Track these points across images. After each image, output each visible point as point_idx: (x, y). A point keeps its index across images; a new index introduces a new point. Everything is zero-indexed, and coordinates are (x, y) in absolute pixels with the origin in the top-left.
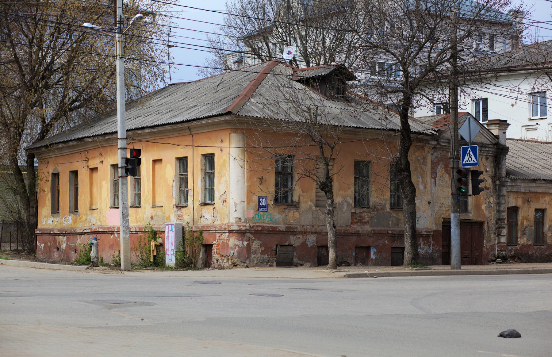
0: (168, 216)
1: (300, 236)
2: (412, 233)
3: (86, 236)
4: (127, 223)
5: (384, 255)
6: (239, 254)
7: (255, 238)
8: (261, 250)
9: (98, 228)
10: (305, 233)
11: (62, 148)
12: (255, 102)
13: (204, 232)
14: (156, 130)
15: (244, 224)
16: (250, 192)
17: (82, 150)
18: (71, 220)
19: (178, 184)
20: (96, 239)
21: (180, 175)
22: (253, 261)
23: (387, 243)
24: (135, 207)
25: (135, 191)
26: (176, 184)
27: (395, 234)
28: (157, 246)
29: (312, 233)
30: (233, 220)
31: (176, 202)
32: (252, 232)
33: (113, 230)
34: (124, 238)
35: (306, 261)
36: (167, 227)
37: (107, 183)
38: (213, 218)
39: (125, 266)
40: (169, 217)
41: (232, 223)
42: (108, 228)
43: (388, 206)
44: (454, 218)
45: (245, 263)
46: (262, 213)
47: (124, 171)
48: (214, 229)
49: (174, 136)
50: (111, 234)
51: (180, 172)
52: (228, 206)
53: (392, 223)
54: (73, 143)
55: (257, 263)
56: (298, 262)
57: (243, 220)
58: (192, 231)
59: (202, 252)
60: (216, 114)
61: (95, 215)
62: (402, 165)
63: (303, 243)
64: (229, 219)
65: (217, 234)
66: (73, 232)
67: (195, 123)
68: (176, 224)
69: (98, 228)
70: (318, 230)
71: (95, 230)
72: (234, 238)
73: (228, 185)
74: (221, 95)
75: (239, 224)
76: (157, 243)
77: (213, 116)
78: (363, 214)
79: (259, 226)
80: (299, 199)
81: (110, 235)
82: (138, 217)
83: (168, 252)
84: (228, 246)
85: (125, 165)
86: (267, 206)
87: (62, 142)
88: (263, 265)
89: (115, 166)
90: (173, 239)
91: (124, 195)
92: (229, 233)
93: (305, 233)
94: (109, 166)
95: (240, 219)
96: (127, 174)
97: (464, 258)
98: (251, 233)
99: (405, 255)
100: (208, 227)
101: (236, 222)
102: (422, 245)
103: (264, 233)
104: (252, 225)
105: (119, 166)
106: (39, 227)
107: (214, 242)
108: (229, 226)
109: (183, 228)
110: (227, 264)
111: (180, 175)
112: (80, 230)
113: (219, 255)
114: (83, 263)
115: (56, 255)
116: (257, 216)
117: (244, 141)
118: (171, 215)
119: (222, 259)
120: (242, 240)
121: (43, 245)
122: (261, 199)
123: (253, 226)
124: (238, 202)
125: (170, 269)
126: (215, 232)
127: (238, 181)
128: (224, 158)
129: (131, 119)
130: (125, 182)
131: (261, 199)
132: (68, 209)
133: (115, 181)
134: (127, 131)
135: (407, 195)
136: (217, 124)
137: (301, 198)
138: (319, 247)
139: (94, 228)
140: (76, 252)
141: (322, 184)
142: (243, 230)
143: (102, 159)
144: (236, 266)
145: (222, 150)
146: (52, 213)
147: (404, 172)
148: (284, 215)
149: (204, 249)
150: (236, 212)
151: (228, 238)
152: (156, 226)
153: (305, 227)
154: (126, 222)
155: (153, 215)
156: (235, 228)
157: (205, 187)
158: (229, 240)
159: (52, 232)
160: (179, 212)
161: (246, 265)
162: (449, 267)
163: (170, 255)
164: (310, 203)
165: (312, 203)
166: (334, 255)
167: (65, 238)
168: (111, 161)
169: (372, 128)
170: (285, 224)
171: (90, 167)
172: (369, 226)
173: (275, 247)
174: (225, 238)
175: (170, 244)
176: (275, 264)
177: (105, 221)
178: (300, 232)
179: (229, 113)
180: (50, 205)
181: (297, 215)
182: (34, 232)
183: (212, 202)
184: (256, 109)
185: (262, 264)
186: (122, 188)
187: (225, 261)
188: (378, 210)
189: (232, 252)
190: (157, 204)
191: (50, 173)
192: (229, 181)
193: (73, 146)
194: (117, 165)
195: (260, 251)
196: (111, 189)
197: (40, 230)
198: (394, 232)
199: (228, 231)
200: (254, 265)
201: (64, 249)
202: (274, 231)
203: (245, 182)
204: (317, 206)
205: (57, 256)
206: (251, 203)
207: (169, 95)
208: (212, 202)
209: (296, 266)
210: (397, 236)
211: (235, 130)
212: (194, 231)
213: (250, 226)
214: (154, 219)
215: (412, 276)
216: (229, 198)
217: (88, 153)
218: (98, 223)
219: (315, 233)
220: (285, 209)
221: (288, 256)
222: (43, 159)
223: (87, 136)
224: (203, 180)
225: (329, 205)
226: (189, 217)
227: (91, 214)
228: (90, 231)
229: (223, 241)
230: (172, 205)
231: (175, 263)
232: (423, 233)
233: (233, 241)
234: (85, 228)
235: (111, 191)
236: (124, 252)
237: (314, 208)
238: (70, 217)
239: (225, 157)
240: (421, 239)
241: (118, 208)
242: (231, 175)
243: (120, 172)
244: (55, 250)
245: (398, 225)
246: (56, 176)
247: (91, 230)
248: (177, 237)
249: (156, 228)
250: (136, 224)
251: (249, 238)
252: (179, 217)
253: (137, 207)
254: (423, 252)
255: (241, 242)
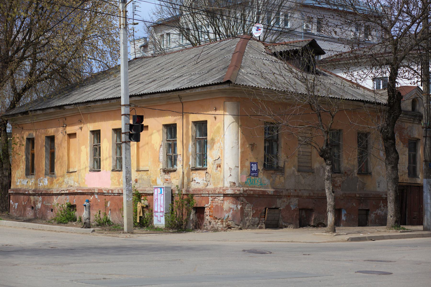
0: (154, 179)
1: (285, 200)
2: (395, 198)
3: (63, 197)
4: (130, 187)
5: (353, 217)
6: (234, 216)
7: (247, 201)
8: (253, 213)
9: (77, 190)
10: (289, 196)
11: (38, 115)
12: (246, 72)
13: (195, 195)
14: (144, 98)
15: (239, 189)
16: (243, 157)
17: (59, 117)
18: (47, 182)
19: (165, 149)
20: (88, 201)
21: (167, 141)
22: (246, 223)
23: (355, 205)
24: (117, 171)
25: (117, 156)
26: (163, 149)
27: (361, 198)
28: (143, 207)
29: (295, 196)
30: (227, 185)
31: (163, 167)
32: (245, 196)
33: (93, 192)
34: (127, 201)
35: (290, 224)
36: (156, 190)
37: (86, 147)
38: (205, 182)
39: (128, 229)
40: (156, 180)
41: (227, 187)
42: (87, 190)
43: (356, 171)
44: (427, 183)
45: (239, 225)
46: (253, 178)
47: (128, 137)
48: (207, 193)
49: (161, 104)
50: (91, 195)
51: (167, 138)
52: (222, 171)
53: (359, 187)
54: (52, 110)
55: (249, 226)
56: (284, 224)
57: (237, 185)
58: (182, 194)
59: (193, 215)
60: (213, 83)
61: (73, 177)
62: (388, 134)
63: (287, 206)
64: (224, 183)
65: (210, 197)
66: (49, 193)
67: (188, 91)
68: (166, 187)
69: (77, 190)
70: (300, 194)
71: (73, 191)
72: (228, 201)
73: (222, 150)
74: (205, 66)
75: (234, 188)
76: (143, 205)
77: (210, 85)
78: (336, 179)
79: (252, 190)
80: (284, 165)
81: (90, 196)
82: (120, 180)
83: (157, 214)
84: (222, 209)
85: (129, 131)
86: (258, 170)
87: (40, 110)
88: (254, 227)
89: (117, 131)
90: (162, 202)
91: (127, 159)
92: (224, 197)
93: (289, 196)
94: (89, 132)
95: (234, 183)
96: (131, 140)
97: (413, 218)
98: (244, 197)
99: (388, 218)
100: (200, 190)
101: (231, 186)
102: (382, 207)
103: (255, 197)
104: (245, 189)
105: (123, 131)
106: (12, 187)
107: (207, 205)
108: (224, 190)
109: (172, 190)
110: (221, 226)
111: (167, 141)
112: (57, 191)
113: (212, 218)
114: (61, 222)
115: (30, 214)
116: (249, 180)
117: (238, 110)
118: (158, 178)
119: (215, 221)
120: (236, 204)
121: (17, 204)
122: (253, 165)
123: (246, 190)
124: (233, 167)
125: (158, 230)
126: (207, 195)
127: (232, 147)
128: (217, 125)
129: (111, 89)
130: (128, 147)
131: (253, 165)
132: (44, 172)
133: (94, 146)
134: (131, 96)
135: (392, 161)
136: (211, 93)
137: (286, 163)
138: (300, 209)
139: (72, 190)
140: (52, 211)
141: (321, 151)
142: (238, 194)
143: (82, 125)
144: (230, 228)
145: (215, 118)
146: (26, 175)
147: (390, 140)
148: (272, 179)
149: (194, 212)
150: (231, 177)
151: (222, 202)
152: (141, 189)
153: (289, 191)
154: (129, 186)
155: (138, 178)
156: (230, 192)
157: (196, 152)
158: (223, 204)
159: (26, 193)
160: (166, 176)
161: (239, 227)
162: (421, 228)
163: (159, 217)
164: (293, 168)
165: (294, 168)
166: (333, 219)
167: (40, 198)
168: (91, 127)
169: (346, 99)
170: (273, 188)
171: (68, 133)
172: (340, 190)
173: (264, 210)
174: (219, 202)
175: (159, 207)
176: (264, 226)
177: (84, 183)
178: (284, 196)
179: (229, 82)
180: (25, 168)
181: (282, 178)
182: (8, 191)
183: (203, 166)
184: (249, 79)
185: (254, 226)
186: (126, 153)
187: (219, 223)
188: (348, 175)
189: (226, 215)
190: (141, 168)
191: (25, 137)
192: (224, 147)
193: (51, 114)
194: (120, 129)
195: (252, 214)
196: (90, 153)
197: (13, 190)
198: (361, 195)
199: (223, 195)
200: (247, 227)
201: (40, 208)
202: (264, 195)
203: (239, 148)
204: (299, 171)
205: (32, 214)
206: (244, 169)
207: (139, 67)
208: (203, 166)
209: (282, 228)
210: (363, 199)
211: (230, 99)
212: (184, 194)
213: (244, 190)
214: (138, 182)
215: (401, 238)
216: (224, 164)
217: (66, 119)
218: (77, 185)
219: (298, 196)
220: (272, 174)
221: (275, 218)
222: (18, 125)
223: (67, 103)
224: (193, 146)
225: (328, 171)
226: (178, 180)
227: (69, 176)
228: (67, 192)
229: (217, 204)
230: (159, 170)
231: (164, 224)
232: (383, 197)
233: (228, 204)
234: (62, 189)
235: (90, 155)
236: (127, 215)
237: (296, 173)
238: (46, 179)
239: (219, 124)
240: (381, 202)
241: (121, 171)
242: (225, 141)
243: (124, 137)
244: (29, 209)
245: (364, 189)
246: (31, 141)
247: (69, 191)
248: (166, 200)
249: (141, 190)
250: (118, 187)
251: (243, 201)
252: (167, 180)
253: (119, 171)
254: (383, 213)
255: (235, 206)
